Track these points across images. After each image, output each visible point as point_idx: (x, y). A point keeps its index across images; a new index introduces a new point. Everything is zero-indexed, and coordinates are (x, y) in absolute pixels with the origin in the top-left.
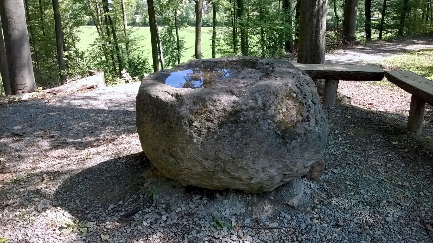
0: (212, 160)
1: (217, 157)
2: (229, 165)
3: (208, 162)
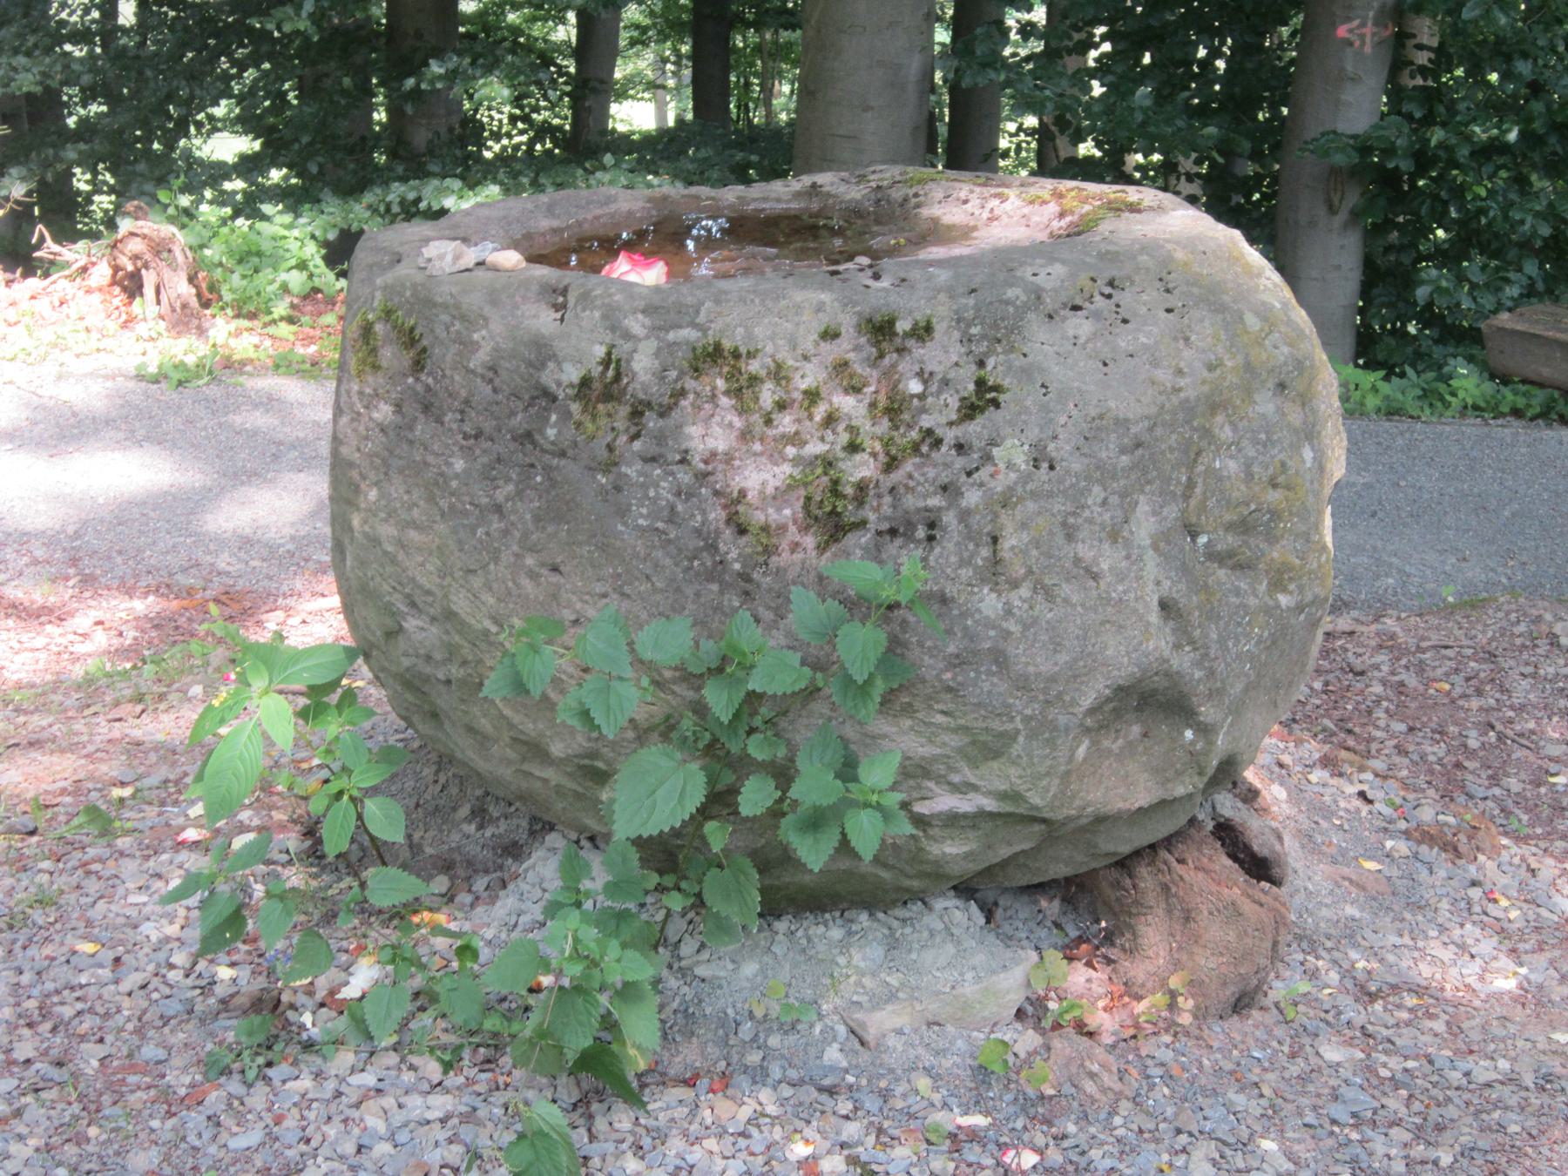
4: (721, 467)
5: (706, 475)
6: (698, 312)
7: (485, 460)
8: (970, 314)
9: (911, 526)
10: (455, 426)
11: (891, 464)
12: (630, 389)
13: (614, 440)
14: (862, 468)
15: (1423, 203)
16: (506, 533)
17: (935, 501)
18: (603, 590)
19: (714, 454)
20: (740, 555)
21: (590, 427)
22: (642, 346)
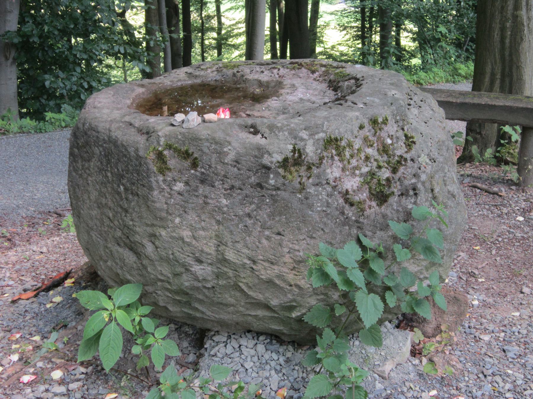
0: (210, 264)
1: (220, 257)
2: (245, 275)
3: (202, 267)
4: (339, 183)
5: (336, 186)
6: (323, 126)
7: (240, 197)
8: (395, 112)
9: (407, 191)
10: (220, 186)
11: (394, 171)
12: (306, 160)
13: (301, 180)
14: (385, 174)
15: (39, 52)
16: (254, 224)
17: (414, 181)
18: (303, 237)
19: (336, 178)
20: (353, 213)
21: (290, 177)
22: (308, 143)
